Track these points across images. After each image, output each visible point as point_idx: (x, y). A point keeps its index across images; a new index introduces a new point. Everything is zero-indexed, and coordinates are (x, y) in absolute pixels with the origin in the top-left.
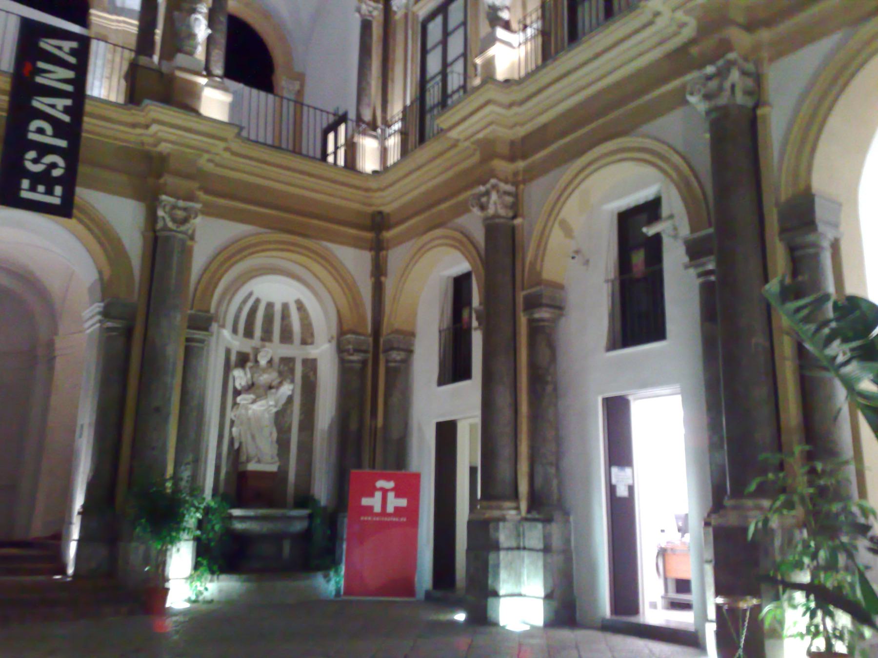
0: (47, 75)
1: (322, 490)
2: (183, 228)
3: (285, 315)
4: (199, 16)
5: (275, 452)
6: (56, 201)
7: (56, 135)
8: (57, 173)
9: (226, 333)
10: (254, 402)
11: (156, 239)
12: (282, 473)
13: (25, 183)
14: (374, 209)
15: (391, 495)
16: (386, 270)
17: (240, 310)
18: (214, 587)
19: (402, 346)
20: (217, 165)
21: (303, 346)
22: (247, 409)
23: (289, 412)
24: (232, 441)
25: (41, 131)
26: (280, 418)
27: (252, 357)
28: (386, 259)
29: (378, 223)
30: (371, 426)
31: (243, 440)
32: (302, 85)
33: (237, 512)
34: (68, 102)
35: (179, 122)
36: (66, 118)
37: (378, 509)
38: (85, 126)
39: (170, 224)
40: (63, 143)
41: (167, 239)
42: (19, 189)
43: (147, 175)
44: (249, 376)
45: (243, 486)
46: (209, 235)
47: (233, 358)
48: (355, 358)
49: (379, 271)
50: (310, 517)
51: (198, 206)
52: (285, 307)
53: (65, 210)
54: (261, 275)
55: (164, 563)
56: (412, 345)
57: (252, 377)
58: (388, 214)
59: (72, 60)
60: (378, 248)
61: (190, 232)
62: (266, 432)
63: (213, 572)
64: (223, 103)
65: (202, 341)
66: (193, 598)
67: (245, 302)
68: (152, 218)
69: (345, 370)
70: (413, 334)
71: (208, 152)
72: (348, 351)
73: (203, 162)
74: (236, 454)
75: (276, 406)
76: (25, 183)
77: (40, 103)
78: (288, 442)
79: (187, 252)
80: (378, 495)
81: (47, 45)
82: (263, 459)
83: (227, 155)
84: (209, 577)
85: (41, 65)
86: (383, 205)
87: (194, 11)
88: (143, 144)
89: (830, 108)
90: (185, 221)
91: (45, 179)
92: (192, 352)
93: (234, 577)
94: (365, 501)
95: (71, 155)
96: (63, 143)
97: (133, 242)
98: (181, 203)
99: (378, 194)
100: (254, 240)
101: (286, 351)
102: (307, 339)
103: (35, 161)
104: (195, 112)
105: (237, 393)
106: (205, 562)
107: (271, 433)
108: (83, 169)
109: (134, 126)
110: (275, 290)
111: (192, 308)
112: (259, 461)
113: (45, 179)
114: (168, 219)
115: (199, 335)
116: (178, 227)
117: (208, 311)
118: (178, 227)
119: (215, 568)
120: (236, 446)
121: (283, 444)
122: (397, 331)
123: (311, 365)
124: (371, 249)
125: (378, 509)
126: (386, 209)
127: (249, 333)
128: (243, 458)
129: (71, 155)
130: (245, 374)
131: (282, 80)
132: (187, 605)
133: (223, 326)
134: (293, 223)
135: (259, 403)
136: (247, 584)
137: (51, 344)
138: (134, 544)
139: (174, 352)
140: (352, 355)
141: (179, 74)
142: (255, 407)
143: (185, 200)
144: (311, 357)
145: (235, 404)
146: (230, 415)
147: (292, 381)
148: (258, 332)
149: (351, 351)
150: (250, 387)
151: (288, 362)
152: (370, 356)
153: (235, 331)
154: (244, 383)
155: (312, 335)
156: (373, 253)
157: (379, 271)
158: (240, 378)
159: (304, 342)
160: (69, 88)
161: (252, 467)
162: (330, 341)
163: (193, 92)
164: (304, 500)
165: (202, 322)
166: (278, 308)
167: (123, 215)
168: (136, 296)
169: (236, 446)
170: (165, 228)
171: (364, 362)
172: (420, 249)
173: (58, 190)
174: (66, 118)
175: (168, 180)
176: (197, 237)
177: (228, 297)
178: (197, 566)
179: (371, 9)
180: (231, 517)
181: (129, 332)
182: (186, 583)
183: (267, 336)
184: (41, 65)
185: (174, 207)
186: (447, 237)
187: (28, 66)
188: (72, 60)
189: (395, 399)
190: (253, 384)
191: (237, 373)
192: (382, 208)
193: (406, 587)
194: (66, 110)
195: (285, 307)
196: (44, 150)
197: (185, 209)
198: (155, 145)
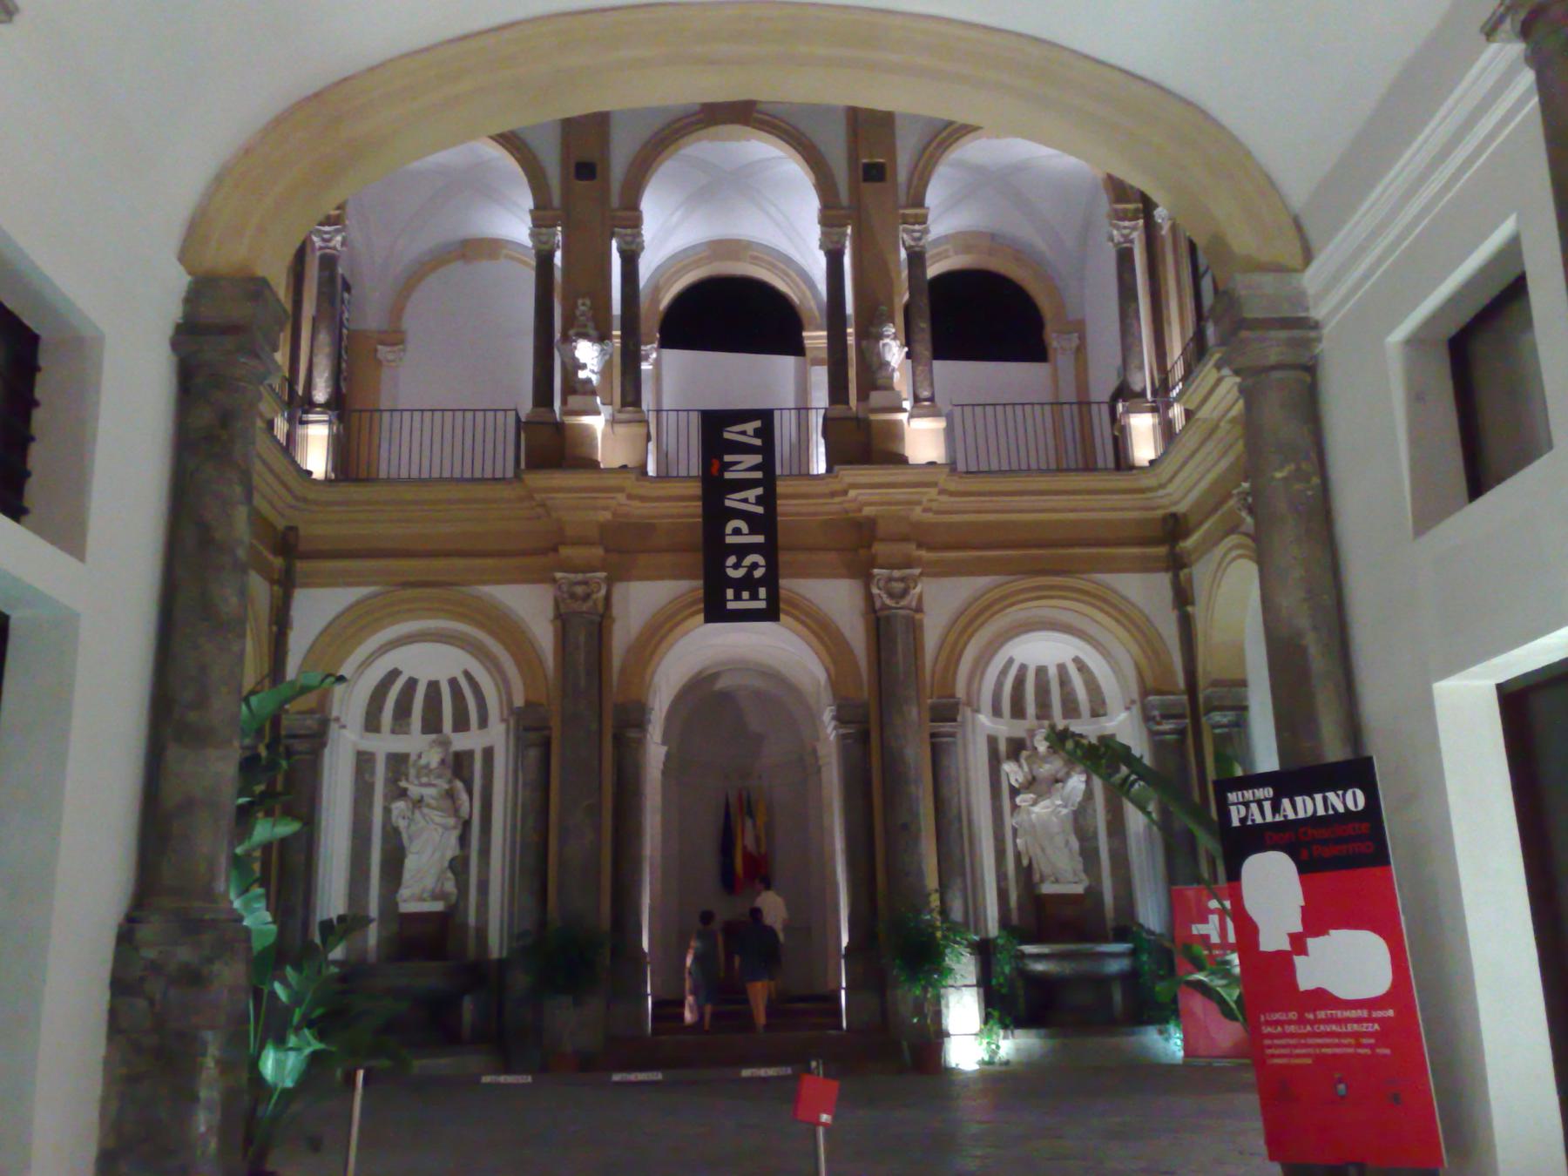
1: (1151, 914)
2: (903, 603)
3: (1064, 681)
4: (887, 341)
5: (1080, 867)
6: (761, 605)
7: (752, 532)
8: (758, 573)
9: (984, 719)
10: (1035, 803)
11: (878, 619)
12: (1094, 893)
13: (730, 593)
14: (1160, 513)
18: (1009, 1046)
19: (1227, 703)
20: (938, 512)
22: (1029, 813)
23: (1090, 811)
24: (1018, 856)
25: (737, 531)
27: (1028, 743)
28: (1190, 580)
29: (1173, 528)
32: (1082, 338)
33: (1029, 949)
34: (759, 491)
35: (877, 480)
36: (760, 510)
38: (779, 509)
39: (888, 602)
40: (760, 539)
41: (888, 618)
42: (725, 600)
43: (858, 545)
44: (1026, 768)
45: (1041, 916)
46: (940, 601)
47: (1003, 747)
49: (1183, 597)
50: (1133, 953)
51: (917, 571)
52: (1062, 668)
53: (770, 614)
54: (1018, 635)
55: (938, 1015)
56: (1245, 698)
57: (1031, 770)
58: (1185, 515)
59: (758, 442)
60: (1176, 564)
61: (914, 604)
62: (1059, 840)
63: (1005, 1027)
64: (932, 430)
65: (952, 735)
66: (986, 1058)
67: (1004, 672)
68: (869, 598)
70: (1243, 683)
71: (919, 503)
72: (1153, 718)
73: (917, 513)
74: (1027, 873)
76: (730, 593)
77: (733, 501)
78: (1096, 851)
81: (731, 434)
82: (1063, 876)
83: (945, 498)
84: (1001, 1033)
85: (728, 458)
86: (1176, 503)
87: (881, 336)
88: (847, 512)
89: (982, 624)
90: (905, 592)
91: (748, 584)
92: (938, 751)
93: (1033, 1032)
94: (1198, 929)
95: (770, 550)
96: (760, 539)
97: (855, 631)
98: (896, 573)
99: (1161, 492)
100: (996, 594)
102: (1099, 710)
103: (736, 566)
104: (901, 460)
105: (1014, 792)
106: (996, 1014)
107: (1067, 842)
108: (784, 557)
109: (833, 494)
110: (1042, 650)
112: (1057, 881)
113: (748, 584)
114: (884, 596)
115: (946, 727)
117: (953, 696)
119: (1008, 1021)
120: (1025, 862)
121: (1089, 855)
122: (1216, 683)
124: (1167, 570)
126: (1181, 508)
127: (1018, 711)
128: (1037, 877)
129: (770, 550)
130: (1020, 766)
131: (1053, 340)
132: (977, 1067)
133: (977, 711)
134: (1044, 559)
135: (1042, 804)
136: (1051, 1043)
137: (815, 751)
138: (899, 992)
139: (916, 754)
140: (1159, 724)
141: (874, 417)
142: (1036, 809)
143: (899, 568)
144: (1108, 732)
145: (1015, 807)
146: (1009, 822)
150: (1031, 783)
153: (997, 711)
154: (1021, 779)
155: (1103, 703)
157: (1183, 597)
158: (1013, 772)
160: (758, 475)
161: (1047, 888)
162: (1128, 709)
163: (894, 433)
164: (1126, 929)
165: (947, 711)
166: (1053, 672)
167: (837, 597)
168: (866, 694)
169: (1025, 862)
170: (885, 607)
171: (1181, 732)
172: (1220, 564)
173: (762, 592)
174: (760, 510)
175: (878, 548)
176: (926, 606)
178: (987, 1019)
179: (1126, 232)
180: (1023, 956)
181: (864, 737)
182: (969, 1038)
184: (728, 458)
185: (890, 579)
186: (1231, 549)
188: (758, 442)
190: (1034, 778)
191: (1008, 767)
192: (1173, 509)
194: (759, 500)
195: (1062, 668)
196: (742, 551)
197: (902, 579)
198: (860, 510)
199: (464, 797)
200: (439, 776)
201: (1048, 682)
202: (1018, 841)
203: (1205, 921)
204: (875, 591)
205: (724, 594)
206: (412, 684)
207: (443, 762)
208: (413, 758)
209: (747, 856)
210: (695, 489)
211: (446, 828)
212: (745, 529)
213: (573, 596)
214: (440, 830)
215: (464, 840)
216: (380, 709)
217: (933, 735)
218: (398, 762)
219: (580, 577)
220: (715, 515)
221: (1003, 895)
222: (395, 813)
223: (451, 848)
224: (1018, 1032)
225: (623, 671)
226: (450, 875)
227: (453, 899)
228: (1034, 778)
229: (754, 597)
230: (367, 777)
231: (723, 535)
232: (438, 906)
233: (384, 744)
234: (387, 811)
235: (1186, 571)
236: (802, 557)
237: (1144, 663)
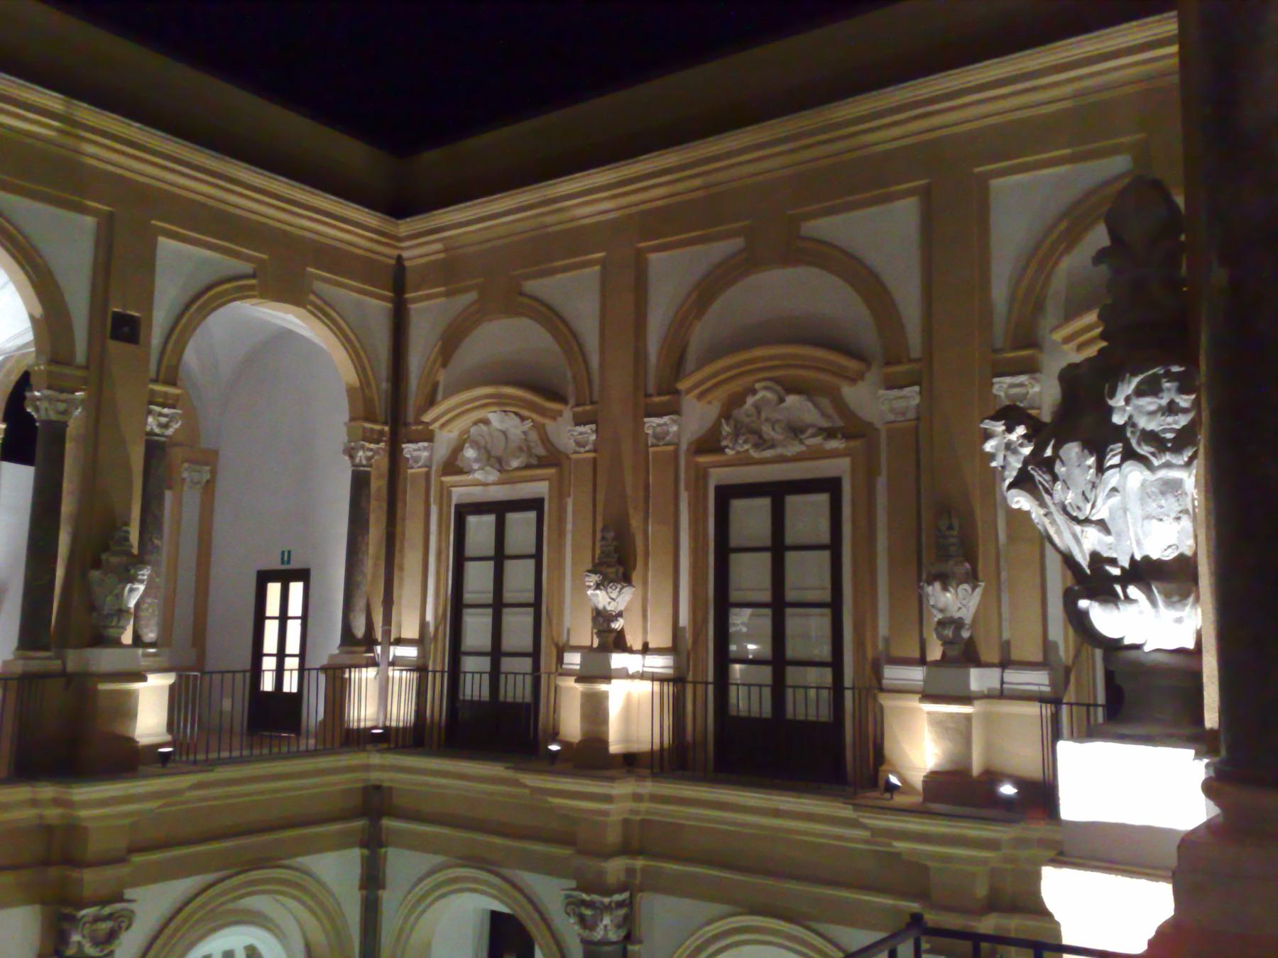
49: (372, 880)
60: (373, 843)
98: (107, 910)
156: (366, 852)
157: (372, 880)
185: (97, 919)
197: (110, 917)
235: (383, 850)
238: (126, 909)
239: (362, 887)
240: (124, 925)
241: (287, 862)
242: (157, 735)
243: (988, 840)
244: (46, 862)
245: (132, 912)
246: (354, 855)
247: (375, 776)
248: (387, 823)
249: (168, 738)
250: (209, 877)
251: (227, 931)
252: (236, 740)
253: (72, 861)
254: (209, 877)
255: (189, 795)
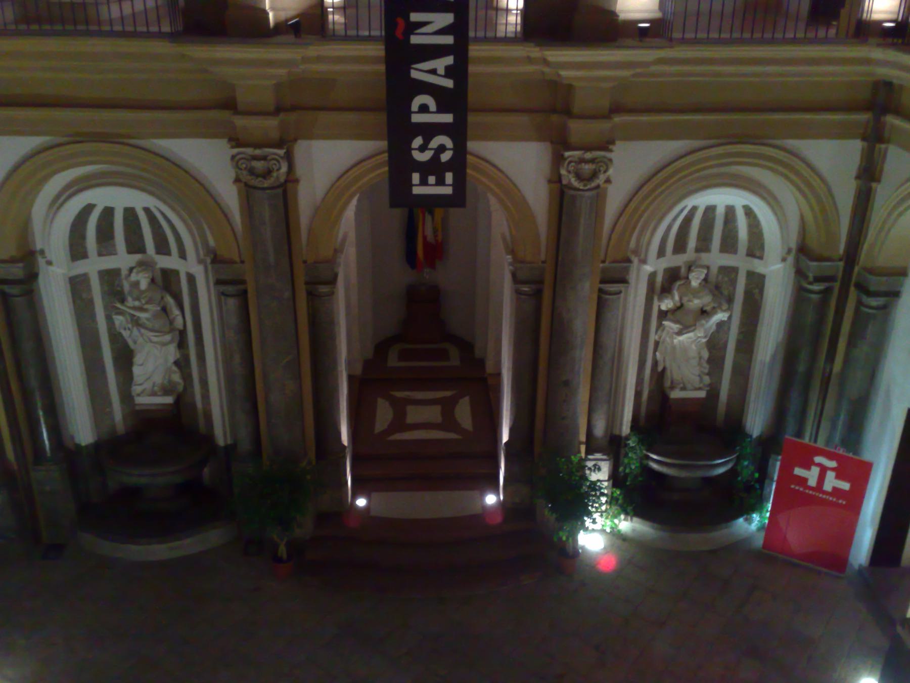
0: (423, 30)
6: (448, 190)
7: (440, 110)
8: (445, 157)
10: (680, 333)
11: (562, 194)
12: (713, 393)
13: (416, 177)
15: (830, 475)
16: (881, 171)
17: (669, 228)
21: (749, 259)
24: (655, 363)
25: (424, 109)
26: (715, 345)
30: (824, 369)
31: (668, 365)
34: (449, 60)
36: (449, 83)
37: (812, 482)
39: (575, 183)
40: (448, 118)
42: (411, 185)
45: (666, 419)
48: (816, 287)
49: (869, 173)
57: (681, 299)
60: (875, 138)
69: (799, 296)
74: (659, 376)
75: (705, 337)
76: (416, 177)
79: (600, 196)
80: (815, 471)
82: (689, 382)
84: (622, 517)
85: (415, 17)
90: (594, 175)
91: (434, 168)
93: (648, 523)
96: (448, 118)
98: (588, 155)
101: (728, 260)
103: (422, 149)
111: (603, 262)
112: (684, 389)
116: (585, 185)
118: (585, 185)
120: (660, 369)
123: (757, 282)
125: (812, 482)
128: (668, 384)
139: (582, 323)
140: (811, 283)
142: (681, 338)
147: (730, 309)
148: (692, 243)
149: (811, 279)
151: (730, 272)
152: (837, 285)
155: (762, 247)
156: (865, 144)
157: (869, 173)
159: (751, 254)
160: (449, 40)
161: (675, 394)
162: (784, 260)
165: (615, 278)
166: (720, 211)
170: (570, 187)
171: (827, 292)
173: (449, 177)
174: (449, 83)
177: (652, 226)
180: (648, 458)
181: (538, 294)
183: (704, 245)
184: (415, 17)
185: (582, 161)
187: (401, 22)
189: (863, 350)
193: (836, 560)
194: (449, 72)
197: (593, 161)
199: (176, 312)
200: (149, 301)
201: (714, 219)
202: (657, 354)
203: (808, 468)
204: (563, 172)
205: (410, 179)
206: (108, 213)
207: (153, 280)
208: (124, 272)
209: (426, 244)
210: (378, 50)
211: (164, 344)
212: (433, 106)
213: (252, 172)
214: (158, 346)
215: (182, 344)
216: (83, 237)
217: (601, 291)
218: (110, 277)
219: (258, 152)
220: (400, 88)
221: (638, 394)
222: (117, 323)
223: (172, 353)
224: (635, 519)
225: (310, 230)
226: (175, 368)
227: (180, 388)
228: (682, 305)
229: (440, 182)
230: (84, 296)
231: (410, 113)
232: (169, 400)
233: (93, 266)
234: (109, 318)
235: (883, 146)
236: (490, 118)
237: (809, 217)
238: (604, 157)
239: (858, 177)
240: (602, 169)
241: (766, 141)
242: (651, 11)
243: (843, 312)
244: (554, 111)
245: (611, 160)
246: (855, 147)
247: (883, 72)
248: (891, 120)
249: (893, 17)
250: (696, 143)
251: (709, 191)
252: (802, 25)
253: (567, 112)
254: (696, 143)
255: (654, 68)
